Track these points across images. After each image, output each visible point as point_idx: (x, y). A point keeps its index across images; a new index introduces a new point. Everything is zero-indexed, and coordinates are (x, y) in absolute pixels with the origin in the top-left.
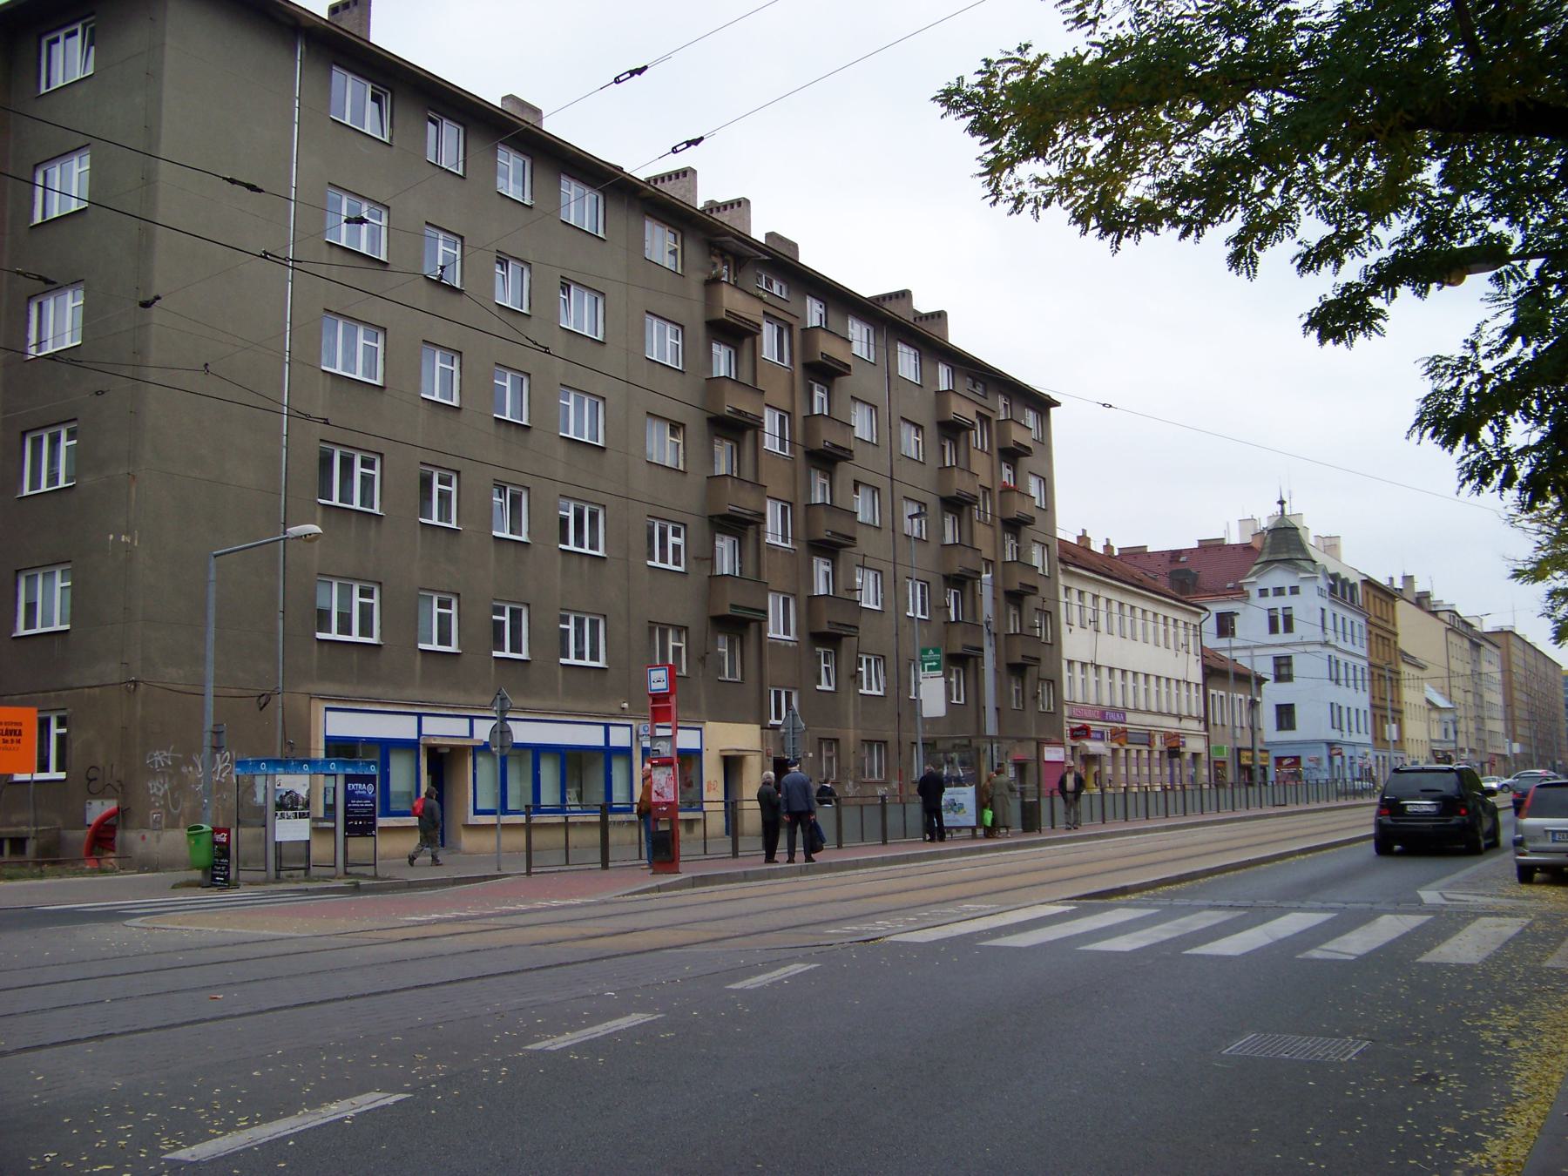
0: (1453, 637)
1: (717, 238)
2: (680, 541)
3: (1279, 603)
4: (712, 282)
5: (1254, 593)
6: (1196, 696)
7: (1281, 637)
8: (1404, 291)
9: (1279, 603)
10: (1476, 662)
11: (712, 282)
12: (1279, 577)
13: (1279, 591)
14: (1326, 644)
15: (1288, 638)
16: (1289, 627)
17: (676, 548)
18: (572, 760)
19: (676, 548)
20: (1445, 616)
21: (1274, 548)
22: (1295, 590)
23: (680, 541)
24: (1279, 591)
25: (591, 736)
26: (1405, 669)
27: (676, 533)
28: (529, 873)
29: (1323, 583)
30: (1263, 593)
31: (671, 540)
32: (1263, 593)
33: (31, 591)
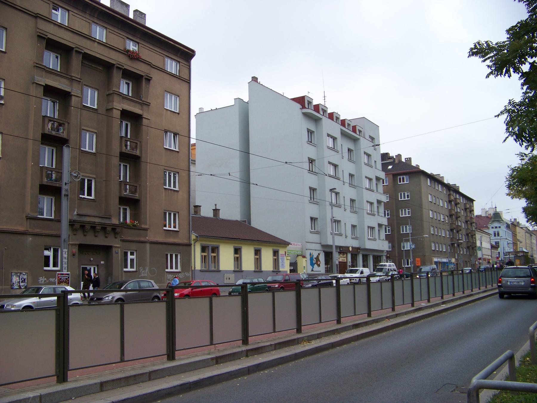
0: (527, 234)
1: (452, 189)
2: (134, 257)
3: (496, 230)
4: (449, 195)
5: (490, 228)
6: (490, 251)
7: (497, 237)
8: (391, 155)
9: (496, 230)
10: (531, 239)
11: (449, 195)
12: (496, 224)
13: (496, 227)
14: (506, 239)
15: (499, 238)
16: (498, 235)
17: (132, 260)
18: (444, 263)
19: (132, 260)
20: (525, 229)
21: (495, 218)
22: (500, 227)
23: (134, 257)
24: (496, 227)
25: (445, 260)
26: (518, 243)
27: (132, 254)
28: (122, 360)
29: (505, 225)
30: (493, 228)
31: (130, 257)
32: (493, 228)
33: (404, 244)
